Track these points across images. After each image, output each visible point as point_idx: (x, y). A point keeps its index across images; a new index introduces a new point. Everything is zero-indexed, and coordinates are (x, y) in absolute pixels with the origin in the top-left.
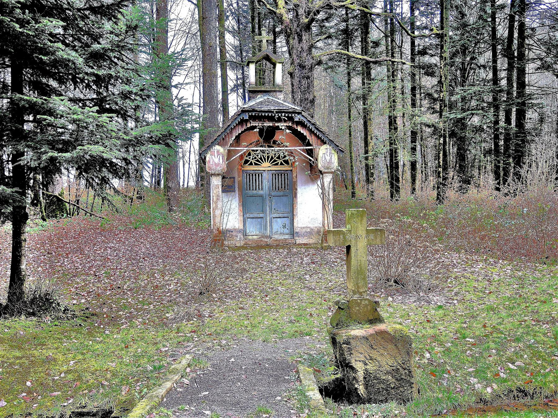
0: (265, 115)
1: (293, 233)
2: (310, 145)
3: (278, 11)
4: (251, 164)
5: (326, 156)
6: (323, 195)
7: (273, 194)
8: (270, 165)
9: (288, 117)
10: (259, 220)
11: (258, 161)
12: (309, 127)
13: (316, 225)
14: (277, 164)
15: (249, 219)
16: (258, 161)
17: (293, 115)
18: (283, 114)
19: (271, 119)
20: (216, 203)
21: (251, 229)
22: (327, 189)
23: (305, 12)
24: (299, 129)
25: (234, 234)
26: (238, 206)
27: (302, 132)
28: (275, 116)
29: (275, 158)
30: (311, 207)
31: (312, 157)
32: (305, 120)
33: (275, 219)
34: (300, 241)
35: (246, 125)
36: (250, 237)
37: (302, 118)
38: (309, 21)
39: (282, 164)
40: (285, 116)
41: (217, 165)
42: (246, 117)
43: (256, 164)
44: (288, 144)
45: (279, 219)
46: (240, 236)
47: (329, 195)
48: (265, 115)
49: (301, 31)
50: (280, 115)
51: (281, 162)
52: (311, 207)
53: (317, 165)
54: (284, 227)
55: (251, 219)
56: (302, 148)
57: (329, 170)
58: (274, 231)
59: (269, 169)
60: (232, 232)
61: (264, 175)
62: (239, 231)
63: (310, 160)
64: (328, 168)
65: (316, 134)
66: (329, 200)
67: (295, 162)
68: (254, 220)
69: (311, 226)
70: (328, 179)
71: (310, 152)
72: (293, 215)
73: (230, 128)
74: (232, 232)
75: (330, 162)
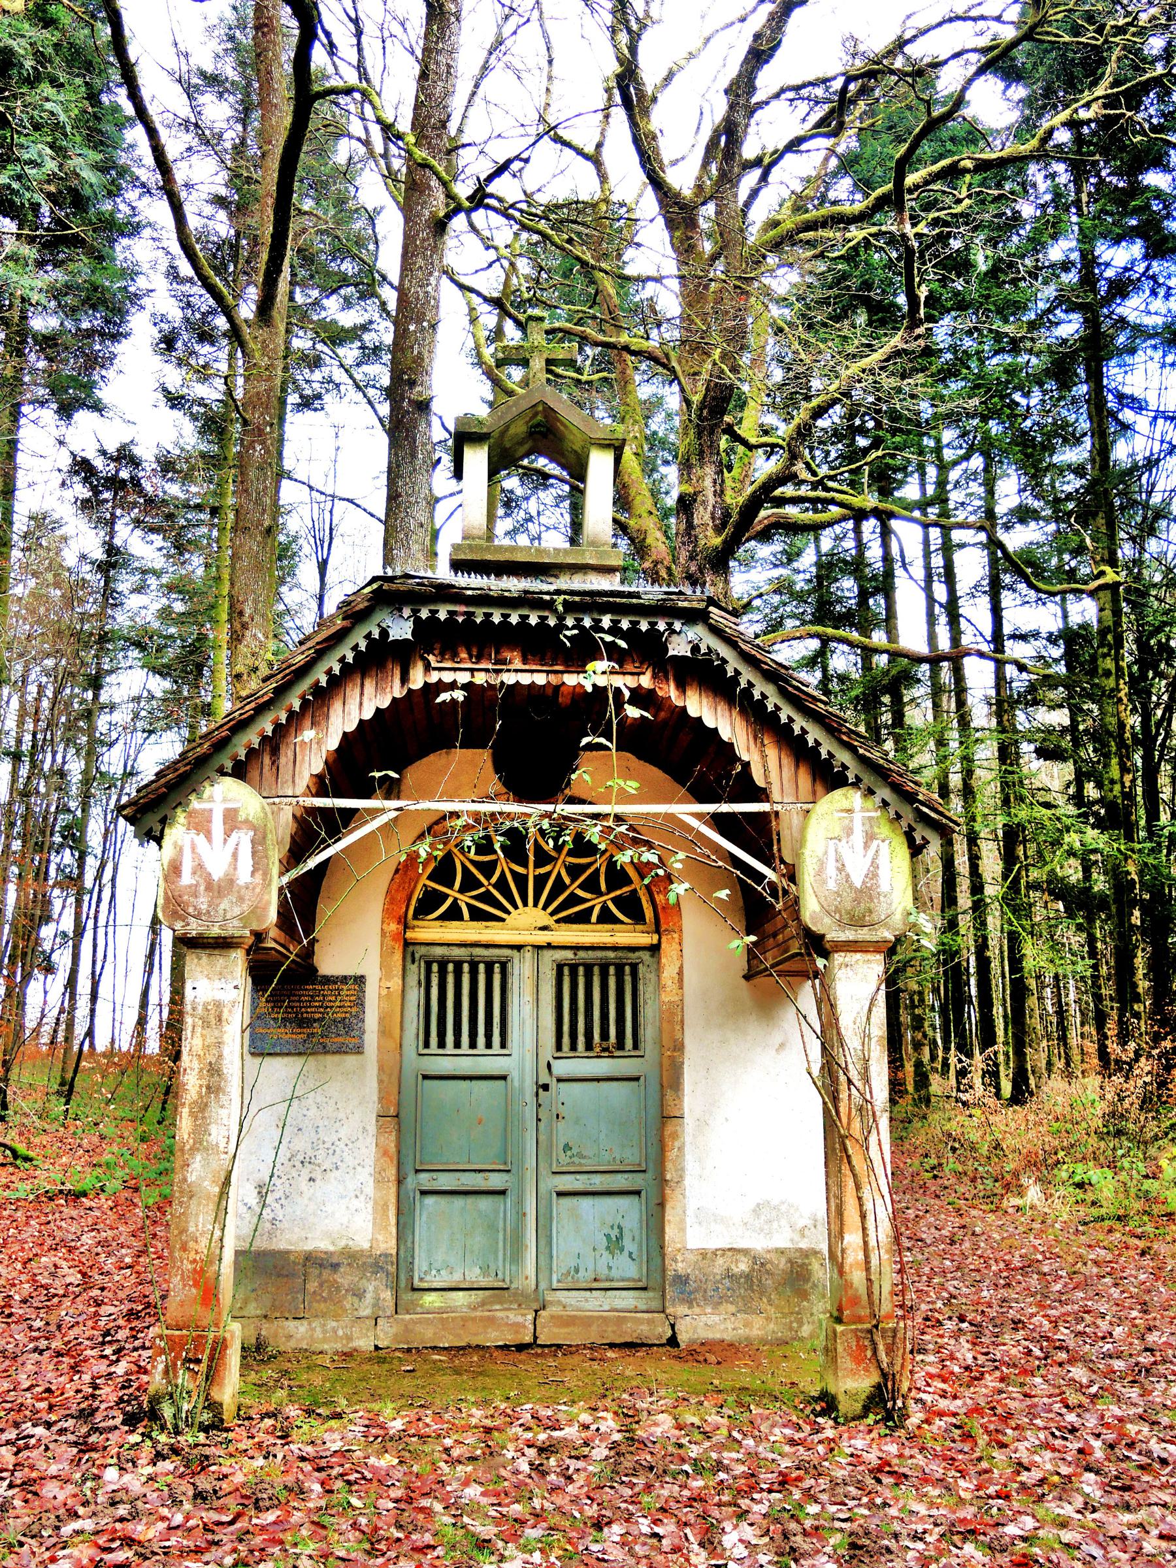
0: (505, 623)
1: (658, 1279)
2: (760, 794)
3: (632, 523)
4: (454, 914)
5: (844, 851)
6: (831, 1077)
7: (562, 1067)
8: (550, 921)
9: (632, 634)
10: (484, 1203)
11: (487, 898)
12: (747, 692)
13: (783, 1239)
14: (583, 918)
15: (430, 1200)
16: (487, 898)
17: (661, 626)
18: (606, 621)
19: (539, 645)
20: (201, 1109)
21: (439, 1257)
22: (852, 1041)
23: (713, 518)
24: (698, 706)
25: (344, 1278)
26: (372, 1128)
27: (709, 722)
28: (561, 627)
29: (575, 888)
30: (759, 1144)
31: (768, 863)
32: (724, 651)
33: (566, 1202)
34: (701, 1323)
35: (404, 679)
36: (430, 1299)
37: (709, 641)
38: (724, 542)
39: (606, 917)
40: (615, 630)
41: (219, 889)
42: (401, 629)
43: (477, 915)
44: (632, 786)
45: (586, 1203)
46: (377, 1291)
47: (866, 1079)
48: (505, 623)
49: (701, 570)
50: (587, 622)
51: (605, 909)
52: (759, 1144)
53: (795, 905)
54: (615, 1244)
55: (443, 1201)
56: (711, 808)
57: (863, 934)
58: (562, 1261)
59: (543, 938)
60: (335, 1267)
61: (522, 969)
62: (373, 1264)
63: (759, 877)
64: (857, 922)
65: (788, 727)
66: (865, 1109)
67: (669, 879)
68: (459, 1202)
69: (759, 1243)
70: (858, 984)
71: (757, 834)
72: (662, 1182)
73: (305, 685)
74: (335, 1267)
75: (867, 893)
